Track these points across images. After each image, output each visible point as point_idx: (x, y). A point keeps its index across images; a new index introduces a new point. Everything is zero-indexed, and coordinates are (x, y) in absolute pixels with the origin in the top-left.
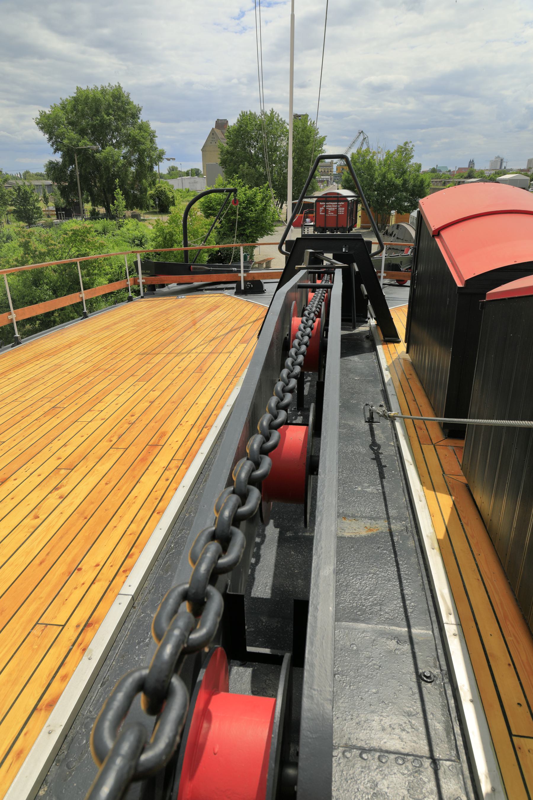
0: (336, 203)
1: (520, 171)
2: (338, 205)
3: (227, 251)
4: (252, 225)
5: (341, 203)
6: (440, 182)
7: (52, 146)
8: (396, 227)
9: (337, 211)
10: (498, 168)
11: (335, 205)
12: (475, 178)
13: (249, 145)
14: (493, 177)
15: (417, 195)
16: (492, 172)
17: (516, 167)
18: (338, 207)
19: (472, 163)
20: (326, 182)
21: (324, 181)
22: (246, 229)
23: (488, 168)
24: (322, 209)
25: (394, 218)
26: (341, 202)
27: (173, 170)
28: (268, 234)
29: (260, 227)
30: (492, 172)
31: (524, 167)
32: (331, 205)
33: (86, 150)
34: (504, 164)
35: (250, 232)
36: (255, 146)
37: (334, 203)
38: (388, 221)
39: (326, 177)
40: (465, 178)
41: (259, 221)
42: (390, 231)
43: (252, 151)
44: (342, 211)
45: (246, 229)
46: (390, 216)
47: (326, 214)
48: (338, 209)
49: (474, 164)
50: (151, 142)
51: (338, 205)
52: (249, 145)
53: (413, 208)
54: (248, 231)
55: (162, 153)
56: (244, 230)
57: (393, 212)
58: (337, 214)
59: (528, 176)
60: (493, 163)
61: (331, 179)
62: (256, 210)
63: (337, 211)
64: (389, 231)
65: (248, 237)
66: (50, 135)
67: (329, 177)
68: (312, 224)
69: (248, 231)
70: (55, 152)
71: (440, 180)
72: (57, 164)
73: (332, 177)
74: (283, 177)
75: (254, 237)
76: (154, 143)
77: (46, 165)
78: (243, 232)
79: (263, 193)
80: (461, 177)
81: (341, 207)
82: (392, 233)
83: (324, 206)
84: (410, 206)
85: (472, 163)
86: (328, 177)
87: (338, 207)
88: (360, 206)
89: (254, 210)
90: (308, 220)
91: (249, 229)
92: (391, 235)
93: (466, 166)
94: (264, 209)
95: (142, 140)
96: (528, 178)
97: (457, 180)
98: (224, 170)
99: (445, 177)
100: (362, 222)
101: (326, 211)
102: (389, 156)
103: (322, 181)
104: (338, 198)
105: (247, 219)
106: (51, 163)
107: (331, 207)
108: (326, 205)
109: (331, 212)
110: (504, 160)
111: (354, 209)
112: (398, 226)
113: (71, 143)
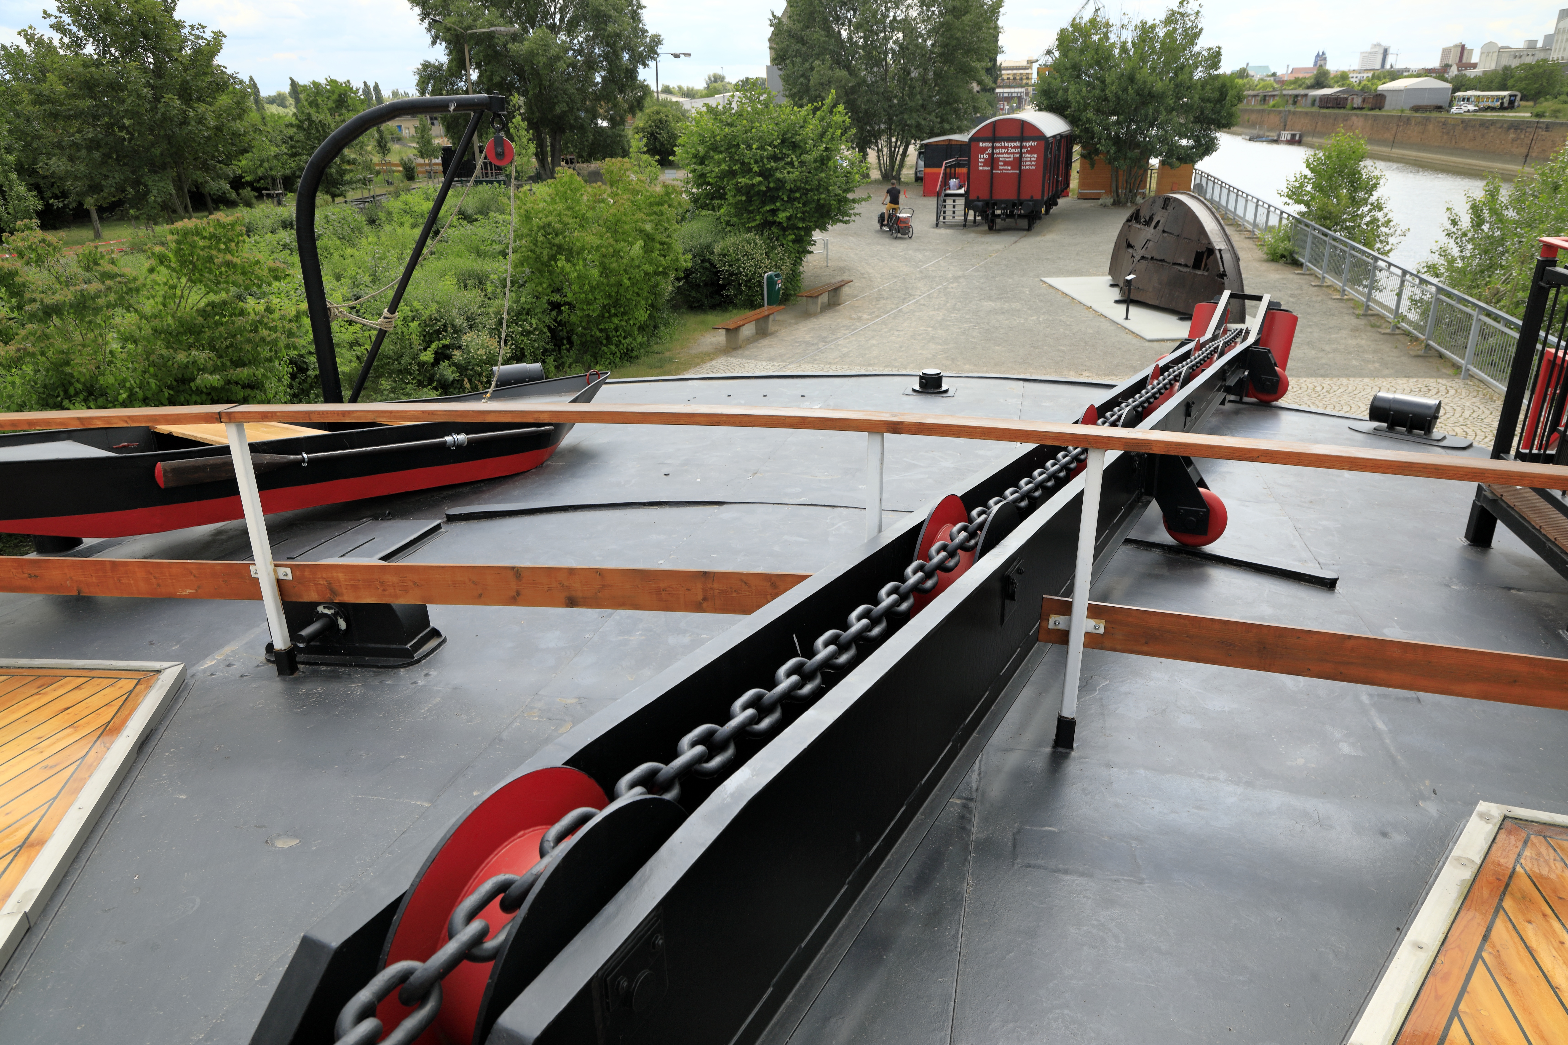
0: (1017, 144)
1: (1427, 73)
2: (1021, 147)
3: (730, 266)
4: (791, 200)
5: (1028, 144)
6: (1254, 96)
7: (429, 30)
8: (1160, 203)
9: (1018, 162)
10: (1378, 66)
11: (1015, 147)
12: (1330, 87)
13: (837, 19)
14: (1369, 84)
15: (1210, 122)
16: (1365, 75)
17: (1416, 65)
18: (1021, 153)
19: (1321, 58)
20: (1016, 100)
21: (1012, 98)
22: (778, 210)
23: (1356, 68)
24: (983, 157)
25: (1155, 176)
26: (1028, 140)
27: (715, 81)
28: (835, 222)
29: (813, 205)
30: (1365, 75)
31: (1435, 63)
32: (1006, 148)
33: (490, 36)
34: (1390, 60)
35: (789, 218)
36: (850, 21)
37: (1013, 144)
38: (1143, 181)
39: (1016, 90)
40: (1309, 87)
41: (811, 190)
42: (1145, 214)
43: (842, 31)
44: (1030, 161)
45: (778, 210)
46: (1146, 170)
47: (992, 169)
48: (1021, 157)
49: (1325, 59)
50: (633, 18)
51: (1021, 147)
52: (837, 19)
53: (1201, 150)
54: (782, 216)
55: (657, 41)
56: (774, 212)
57: (1154, 162)
58: (1020, 169)
59: (1446, 80)
60: (1366, 56)
61: (1027, 94)
62: (802, 163)
63: (1018, 162)
64: (1142, 214)
65: (784, 229)
66: (423, 8)
67: (1023, 90)
68: (962, 191)
69: (782, 216)
70: (434, 43)
71: (1255, 93)
72: (439, 68)
73: (1030, 89)
74: (910, 87)
75: (798, 228)
76: (640, 21)
77: (419, 72)
78: (770, 218)
79: (822, 119)
80: (1300, 86)
81: (1028, 152)
82: (1151, 219)
83: (990, 151)
84: (1192, 148)
85: (1321, 58)
86: (1020, 90)
87: (1021, 153)
88: (1077, 148)
89: (796, 163)
90: (953, 182)
91: (784, 211)
92: (1147, 223)
93: (1310, 64)
94: (823, 161)
95: (613, 13)
96: (1449, 86)
97: (1291, 92)
98: (781, 72)
99: (1265, 87)
100: (1082, 184)
101: (992, 161)
102: (1146, 32)
103: (1009, 99)
104: (1025, 131)
105: (781, 182)
106: (426, 66)
107: (1006, 152)
108: (993, 148)
109: (1006, 163)
110: (1390, 51)
111: (1062, 158)
112: (1167, 200)
113: (461, 22)
